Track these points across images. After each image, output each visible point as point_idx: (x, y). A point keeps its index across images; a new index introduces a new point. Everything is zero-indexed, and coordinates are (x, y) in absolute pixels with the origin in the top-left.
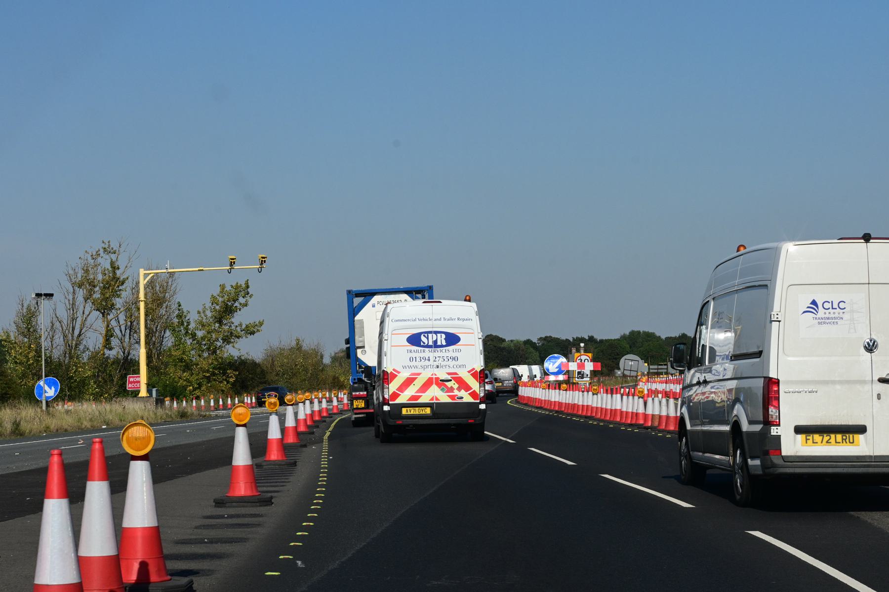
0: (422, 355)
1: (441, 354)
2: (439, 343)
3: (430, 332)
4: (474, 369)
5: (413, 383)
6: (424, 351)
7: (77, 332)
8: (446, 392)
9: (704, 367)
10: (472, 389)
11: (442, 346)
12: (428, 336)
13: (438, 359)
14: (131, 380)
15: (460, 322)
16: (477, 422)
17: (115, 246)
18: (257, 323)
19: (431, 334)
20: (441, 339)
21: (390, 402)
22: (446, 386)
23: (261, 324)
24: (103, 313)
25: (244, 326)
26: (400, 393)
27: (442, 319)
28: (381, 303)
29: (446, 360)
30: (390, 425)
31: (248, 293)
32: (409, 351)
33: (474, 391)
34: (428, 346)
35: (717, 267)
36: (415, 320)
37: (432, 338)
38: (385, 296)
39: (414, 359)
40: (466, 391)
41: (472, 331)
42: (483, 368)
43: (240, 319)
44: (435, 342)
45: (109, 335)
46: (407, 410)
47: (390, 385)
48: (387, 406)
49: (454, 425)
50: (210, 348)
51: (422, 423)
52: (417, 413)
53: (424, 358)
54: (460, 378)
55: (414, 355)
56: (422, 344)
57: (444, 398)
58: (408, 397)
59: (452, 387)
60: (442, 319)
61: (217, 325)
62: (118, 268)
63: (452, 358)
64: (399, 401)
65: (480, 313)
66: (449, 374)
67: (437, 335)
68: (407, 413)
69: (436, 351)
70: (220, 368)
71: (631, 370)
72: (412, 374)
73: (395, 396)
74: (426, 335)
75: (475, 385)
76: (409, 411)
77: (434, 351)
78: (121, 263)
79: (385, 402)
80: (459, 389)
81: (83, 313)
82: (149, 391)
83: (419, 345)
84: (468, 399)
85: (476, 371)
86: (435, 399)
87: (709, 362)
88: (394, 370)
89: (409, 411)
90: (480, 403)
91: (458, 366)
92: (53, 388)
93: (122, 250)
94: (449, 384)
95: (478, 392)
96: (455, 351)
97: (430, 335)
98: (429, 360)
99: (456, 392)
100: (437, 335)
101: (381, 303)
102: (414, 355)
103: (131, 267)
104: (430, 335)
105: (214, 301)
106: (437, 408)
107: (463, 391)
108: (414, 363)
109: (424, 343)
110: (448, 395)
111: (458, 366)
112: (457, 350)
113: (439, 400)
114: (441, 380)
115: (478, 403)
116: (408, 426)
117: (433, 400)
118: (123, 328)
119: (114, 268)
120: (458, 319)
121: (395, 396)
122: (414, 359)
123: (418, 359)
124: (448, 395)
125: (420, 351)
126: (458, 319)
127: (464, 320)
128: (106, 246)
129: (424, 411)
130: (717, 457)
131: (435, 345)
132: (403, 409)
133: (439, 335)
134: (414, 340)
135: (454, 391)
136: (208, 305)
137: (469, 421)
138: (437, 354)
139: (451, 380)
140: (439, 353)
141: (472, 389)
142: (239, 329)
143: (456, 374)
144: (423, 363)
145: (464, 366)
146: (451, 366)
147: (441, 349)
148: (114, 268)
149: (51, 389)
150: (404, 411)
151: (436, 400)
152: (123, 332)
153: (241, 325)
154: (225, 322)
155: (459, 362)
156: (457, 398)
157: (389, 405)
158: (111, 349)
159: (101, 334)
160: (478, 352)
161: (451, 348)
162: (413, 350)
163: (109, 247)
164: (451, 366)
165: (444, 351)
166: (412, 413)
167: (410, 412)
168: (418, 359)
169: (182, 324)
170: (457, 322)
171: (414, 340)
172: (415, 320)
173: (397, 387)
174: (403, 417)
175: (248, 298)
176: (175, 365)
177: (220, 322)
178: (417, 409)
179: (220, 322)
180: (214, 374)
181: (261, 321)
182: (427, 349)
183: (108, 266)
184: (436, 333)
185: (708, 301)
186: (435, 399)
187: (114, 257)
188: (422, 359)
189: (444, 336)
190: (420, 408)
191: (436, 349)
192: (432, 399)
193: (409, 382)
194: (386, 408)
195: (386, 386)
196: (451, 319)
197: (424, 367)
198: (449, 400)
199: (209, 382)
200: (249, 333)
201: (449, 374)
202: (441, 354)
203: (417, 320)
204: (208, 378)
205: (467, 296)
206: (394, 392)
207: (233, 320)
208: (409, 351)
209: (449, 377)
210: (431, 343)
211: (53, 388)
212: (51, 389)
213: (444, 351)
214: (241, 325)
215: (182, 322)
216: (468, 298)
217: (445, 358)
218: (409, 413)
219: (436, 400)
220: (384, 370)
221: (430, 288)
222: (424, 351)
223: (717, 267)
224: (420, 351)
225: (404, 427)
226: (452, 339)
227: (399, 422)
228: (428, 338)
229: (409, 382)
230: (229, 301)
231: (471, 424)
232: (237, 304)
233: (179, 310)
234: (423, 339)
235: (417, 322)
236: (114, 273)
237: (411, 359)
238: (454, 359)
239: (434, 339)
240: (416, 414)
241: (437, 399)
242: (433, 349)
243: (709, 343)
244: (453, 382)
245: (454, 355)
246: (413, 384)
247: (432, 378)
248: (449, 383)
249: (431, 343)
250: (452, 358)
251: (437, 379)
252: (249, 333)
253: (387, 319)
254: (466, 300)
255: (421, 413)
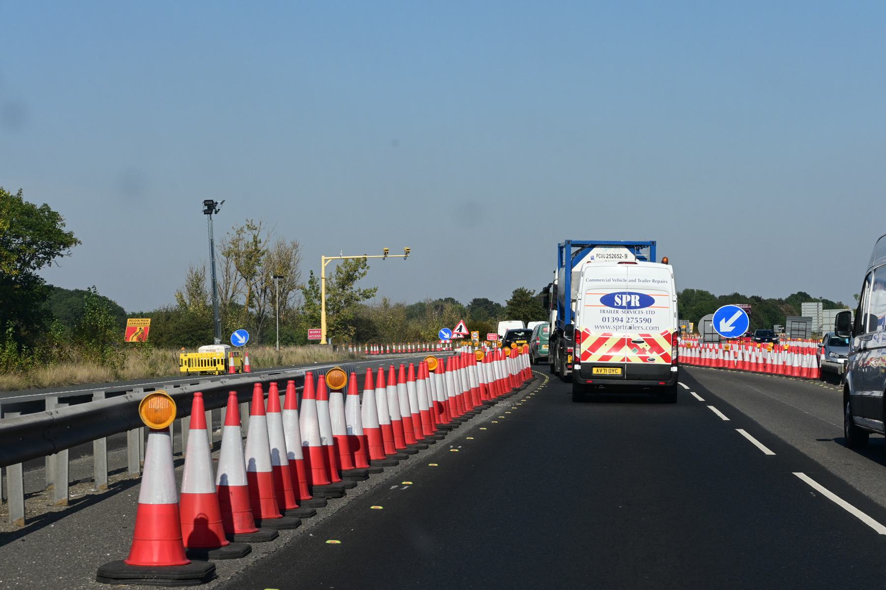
0: (615, 316)
1: (634, 316)
2: (633, 304)
3: (625, 293)
4: (667, 331)
5: (605, 344)
6: (617, 312)
7: (230, 294)
8: (637, 354)
9: (864, 335)
10: (664, 351)
11: (636, 307)
12: (622, 297)
13: (631, 320)
14: (311, 332)
15: (641, 283)
16: (668, 385)
17: (256, 224)
18: (373, 289)
19: (625, 296)
20: (635, 301)
21: (581, 362)
22: (638, 347)
23: (375, 290)
24: (246, 279)
25: (362, 291)
26: (591, 352)
27: (637, 280)
28: (600, 256)
29: (639, 321)
30: (582, 384)
31: (366, 265)
32: (602, 311)
33: (666, 353)
34: (621, 307)
35: (879, 239)
36: (609, 280)
37: (626, 299)
38: (605, 249)
39: (607, 319)
40: (658, 353)
41: (667, 294)
42: (676, 330)
43: (358, 286)
44: (629, 303)
45: (251, 297)
46: (598, 370)
47: (581, 345)
48: (578, 365)
49: (647, 386)
50: (334, 308)
51: (611, 384)
52: (608, 373)
53: (617, 319)
54: (653, 340)
55: (607, 315)
56: (616, 305)
57: (635, 358)
58: (599, 357)
59: (644, 349)
60: (637, 280)
61: (341, 290)
62: (260, 242)
63: (645, 320)
64: (590, 360)
65: (675, 276)
66: (642, 335)
67: (631, 296)
68: (598, 373)
69: (630, 312)
70: (341, 324)
71: (712, 334)
72: (605, 334)
73: (586, 355)
74: (620, 296)
75: (667, 348)
76: (599, 371)
77: (628, 312)
78: (261, 237)
79: (576, 361)
80: (651, 351)
81: (236, 279)
82: (327, 340)
83: (614, 307)
84: (659, 361)
85: (669, 333)
86: (626, 360)
87: (870, 330)
88: (586, 329)
89: (599, 371)
90: (672, 366)
91: (651, 328)
92: (244, 337)
93: (262, 227)
94: (641, 346)
95: (670, 354)
96: (648, 312)
97: (624, 296)
98: (622, 321)
99: (648, 354)
100: (631, 296)
101: (600, 256)
102: (607, 315)
103: (269, 241)
104: (624, 296)
105: (339, 271)
106: (629, 369)
107: (655, 353)
108: (607, 324)
109: (617, 304)
110: (639, 357)
111: (651, 328)
112: (651, 312)
113: (630, 361)
114: (633, 342)
115: (669, 365)
116: (598, 385)
117: (624, 361)
118: (260, 291)
119: (256, 242)
120: (653, 281)
121: (586, 355)
122: (607, 319)
123: (611, 320)
124: (639, 357)
125: (613, 312)
126: (653, 281)
127: (659, 282)
128: (249, 224)
129: (614, 371)
130: (876, 421)
131: (629, 306)
132: (594, 368)
133: (633, 296)
134: (608, 300)
135: (646, 353)
136: (334, 273)
137: (660, 383)
138: (630, 315)
139: (643, 342)
140: (632, 314)
141: (664, 351)
142: (358, 294)
143: (648, 335)
144: (616, 324)
145: (657, 328)
146: (644, 328)
147: (635, 310)
148: (256, 242)
149: (242, 338)
150: (595, 371)
151: (627, 361)
152: (260, 294)
153: (359, 290)
154: (346, 287)
155: (652, 324)
156: (649, 360)
157: (580, 364)
158: (253, 307)
159: (245, 295)
160: (672, 315)
161: (645, 309)
162: (606, 311)
163: (251, 225)
164: (644, 328)
165: (637, 312)
166: (602, 373)
167: (601, 372)
168: (611, 320)
169: (313, 289)
170: (651, 284)
171: (608, 300)
172: (609, 280)
173: (588, 347)
174: (593, 376)
175: (366, 269)
176: (307, 321)
177: (343, 288)
178: (608, 369)
179: (343, 288)
180: (338, 329)
181: (376, 288)
182: (620, 310)
183: (251, 240)
184: (630, 294)
185: (870, 272)
186: (626, 360)
187: (255, 232)
188: (614, 319)
189: (638, 297)
190: (611, 368)
191: (630, 310)
192: (623, 360)
193: (601, 342)
194: (577, 367)
195: (577, 345)
196: (646, 281)
197: (617, 328)
198: (641, 362)
199: (334, 335)
200: (366, 297)
201: (642, 335)
202: (634, 316)
203: (611, 280)
204: (333, 331)
205: (664, 258)
206: (586, 351)
207: (353, 286)
208: (602, 311)
209: (641, 339)
210: (624, 304)
211: (244, 337)
212: (242, 338)
213: (637, 312)
214: (359, 290)
215: (314, 287)
216: (665, 260)
217: (638, 319)
218: (599, 373)
219: (627, 361)
220: (576, 330)
221: (652, 244)
222: (617, 312)
223: (879, 239)
224: (613, 312)
225: (592, 386)
226: (646, 301)
227: (590, 381)
228: (621, 299)
229: (601, 342)
230: (351, 271)
231: (662, 387)
232: (357, 274)
233: (311, 277)
234: (617, 299)
235: (612, 283)
236: (256, 245)
237: (604, 320)
238: (647, 320)
239: (628, 300)
240: (607, 375)
241: (628, 360)
242: (626, 310)
243: (870, 311)
244: (645, 343)
245: (647, 317)
246: (647, 345)
247: (625, 339)
248: (642, 344)
249: (624, 304)
250: (645, 320)
251: (629, 340)
252: (366, 297)
253: (582, 278)
254: (663, 262)
255: (612, 373)
